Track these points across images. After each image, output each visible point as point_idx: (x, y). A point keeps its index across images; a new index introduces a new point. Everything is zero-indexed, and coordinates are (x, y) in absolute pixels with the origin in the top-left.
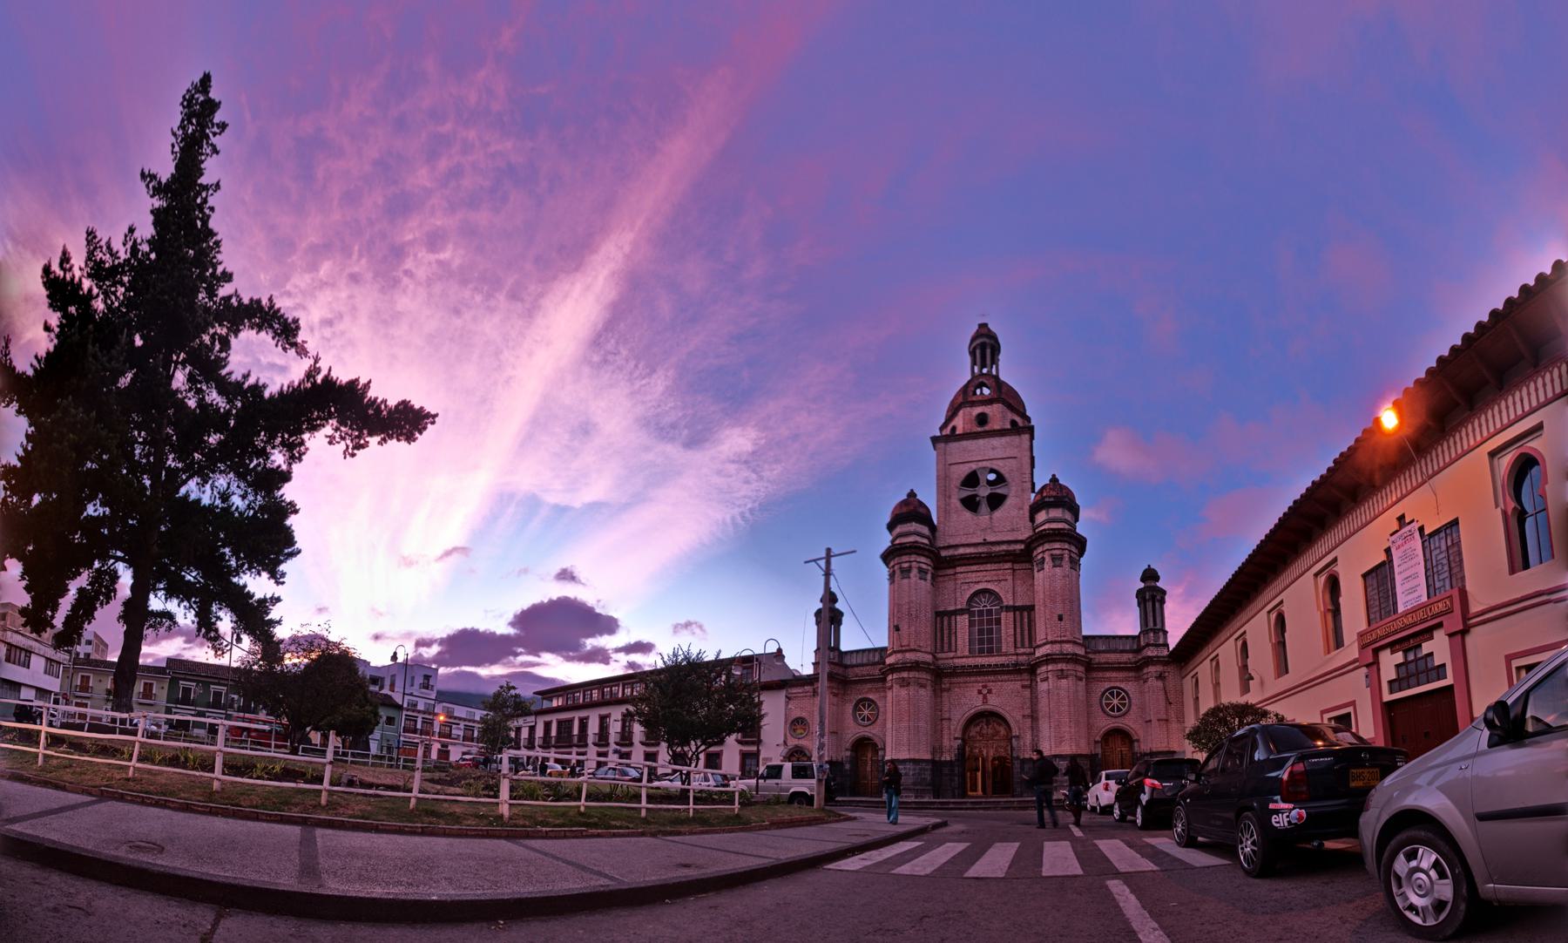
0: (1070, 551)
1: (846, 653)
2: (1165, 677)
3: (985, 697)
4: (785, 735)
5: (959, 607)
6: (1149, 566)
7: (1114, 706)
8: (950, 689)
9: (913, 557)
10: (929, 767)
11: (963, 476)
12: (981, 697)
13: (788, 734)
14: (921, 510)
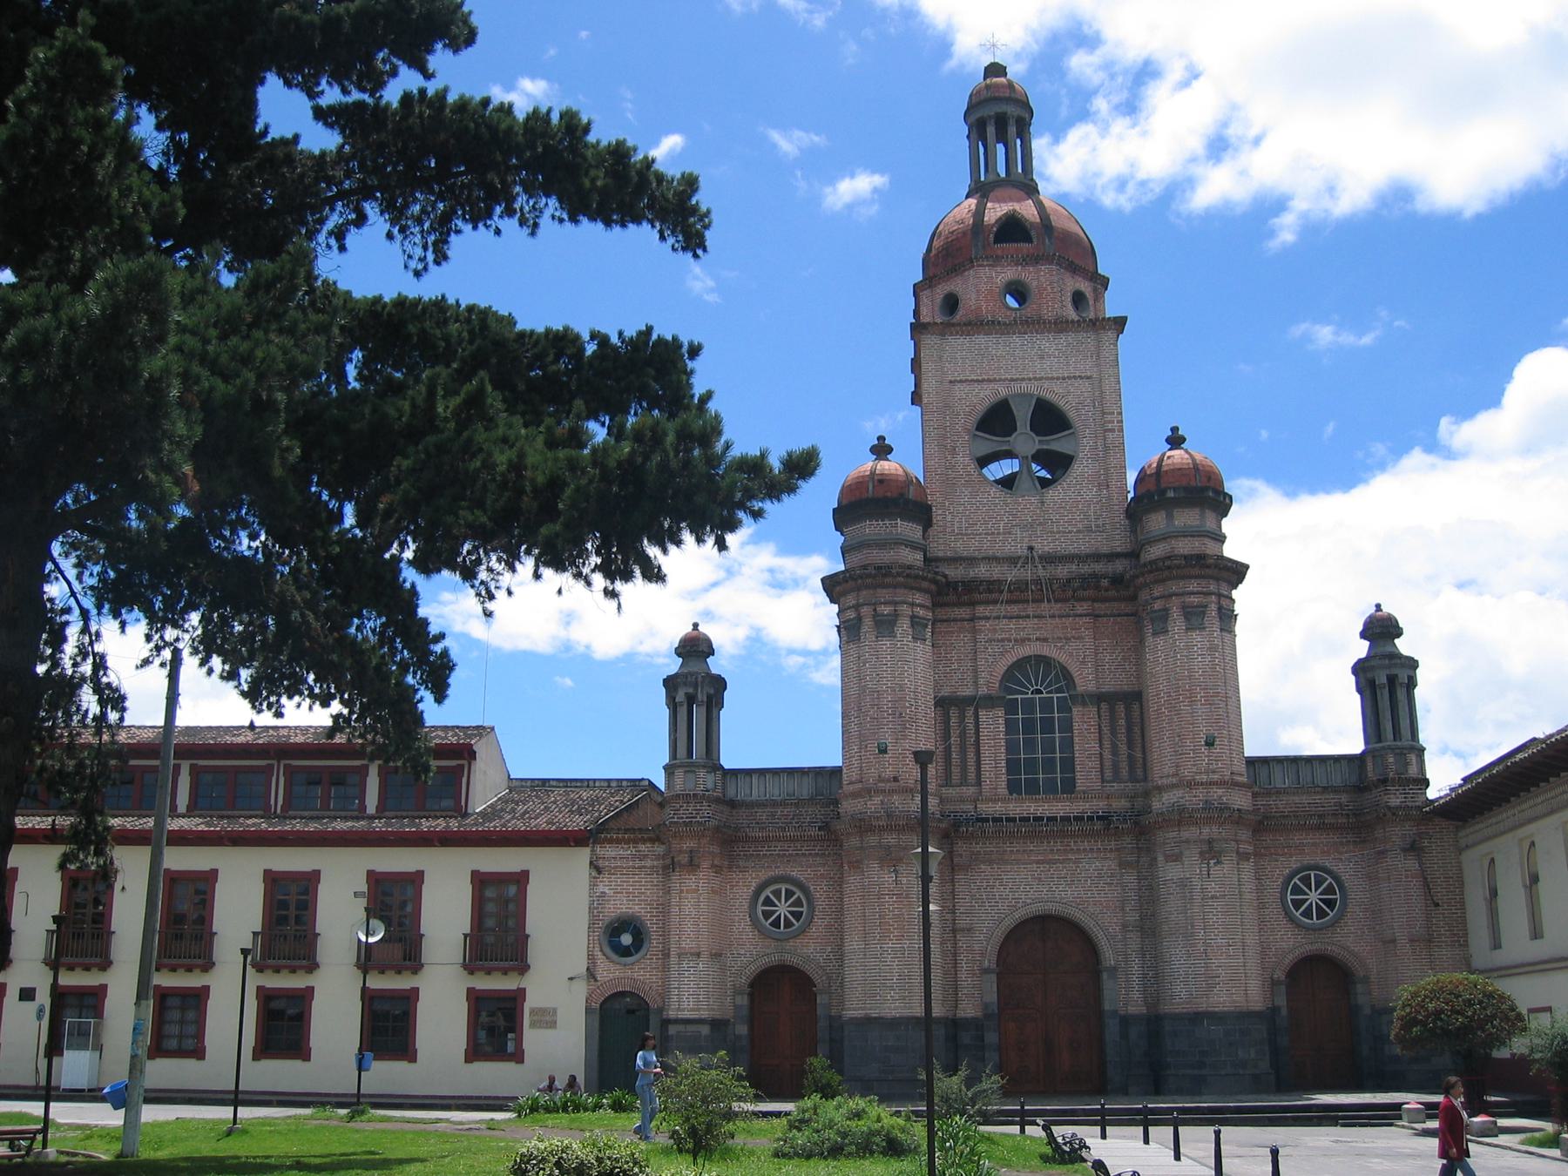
1: (735, 773)
5: (983, 691)
6: (1378, 607)
7: (792, 913)
9: (901, 594)
11: (981, 409)
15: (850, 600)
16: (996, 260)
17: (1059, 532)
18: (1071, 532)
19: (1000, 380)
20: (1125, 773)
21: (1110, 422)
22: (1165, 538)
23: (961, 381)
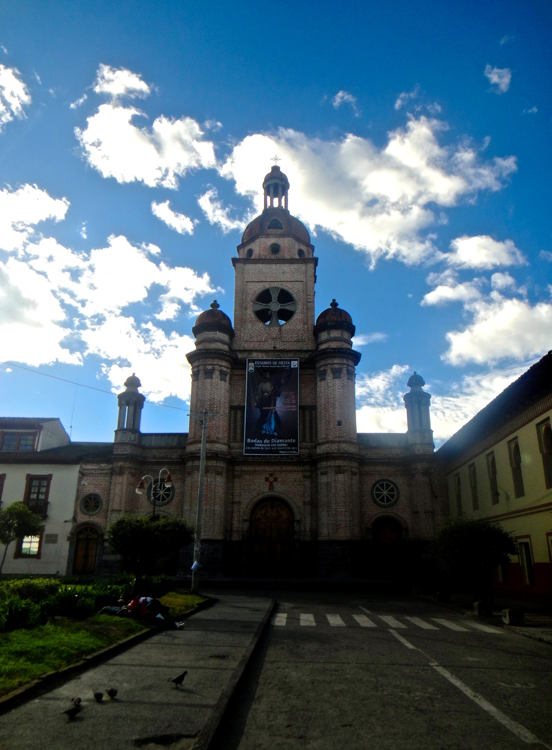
0: (348, 365)
3: (271, 485)
8: (241, 475)
11: (258, 292)
13: (79, 511)
14: (224, 322)
15: (196, 364)
16: (268, 236)
17: (286, 341)
18: (291, 341)
19: (266, 281)
20: (308, 438)
21: (309, 299)
22: (326, 341)
23: (251, 282)
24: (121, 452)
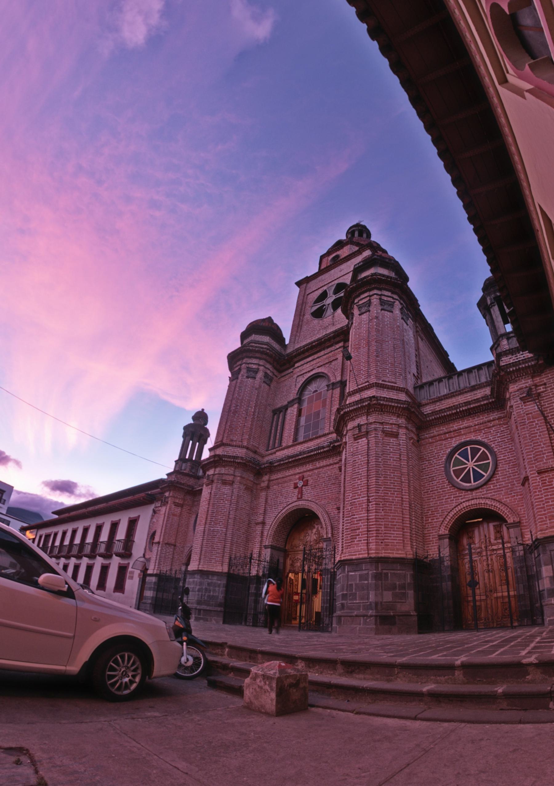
2: (539, 395)
4: (145, 550)
10: (224, 582)
12: (296, 491)
24: (389, 382)
